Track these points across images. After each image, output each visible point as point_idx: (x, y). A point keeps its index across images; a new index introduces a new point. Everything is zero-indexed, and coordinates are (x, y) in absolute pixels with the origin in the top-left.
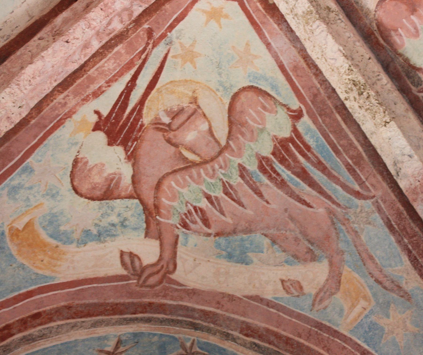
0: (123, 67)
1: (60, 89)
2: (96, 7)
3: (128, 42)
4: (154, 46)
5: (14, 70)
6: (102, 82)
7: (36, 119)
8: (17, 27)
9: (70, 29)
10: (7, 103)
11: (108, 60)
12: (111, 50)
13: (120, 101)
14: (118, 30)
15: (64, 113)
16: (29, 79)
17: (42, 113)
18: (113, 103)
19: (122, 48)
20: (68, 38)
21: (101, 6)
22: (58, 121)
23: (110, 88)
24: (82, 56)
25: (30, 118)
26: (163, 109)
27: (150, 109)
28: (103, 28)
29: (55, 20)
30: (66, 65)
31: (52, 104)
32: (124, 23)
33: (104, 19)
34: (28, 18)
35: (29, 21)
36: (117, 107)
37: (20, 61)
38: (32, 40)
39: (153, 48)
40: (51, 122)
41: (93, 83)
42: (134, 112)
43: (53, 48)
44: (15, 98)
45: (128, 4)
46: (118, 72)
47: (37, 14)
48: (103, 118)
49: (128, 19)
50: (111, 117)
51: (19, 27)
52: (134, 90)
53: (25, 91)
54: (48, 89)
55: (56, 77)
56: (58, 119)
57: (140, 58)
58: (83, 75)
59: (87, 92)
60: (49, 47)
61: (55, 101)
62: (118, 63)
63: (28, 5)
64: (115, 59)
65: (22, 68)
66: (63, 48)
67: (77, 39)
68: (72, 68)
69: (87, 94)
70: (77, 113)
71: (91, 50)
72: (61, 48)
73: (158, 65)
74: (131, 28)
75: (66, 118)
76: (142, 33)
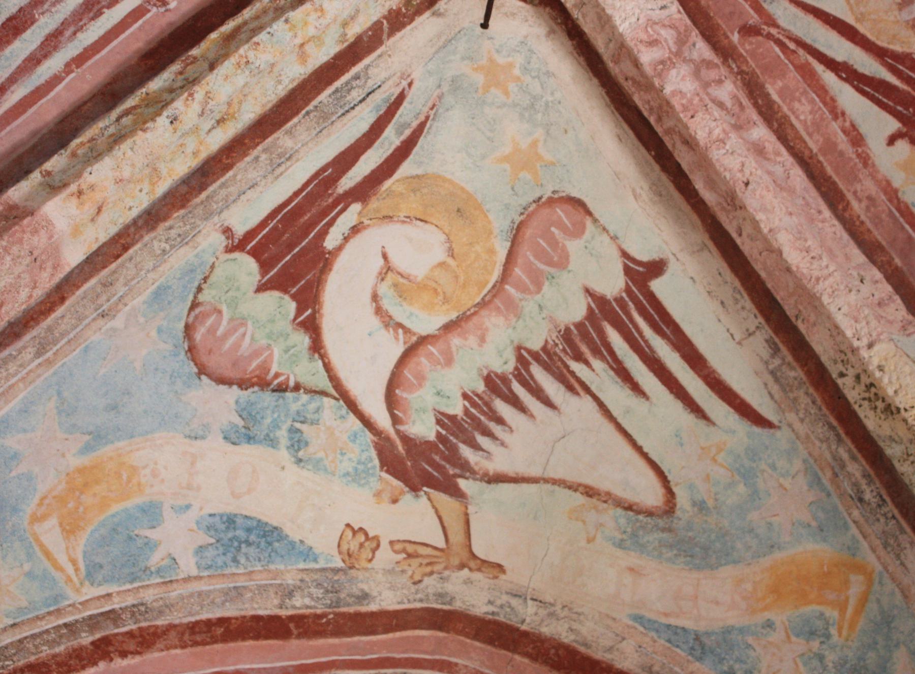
0: (809, 85)
1: (840, 207)
2: (686, 127)
3: (762, 74)
4: (775, 25)
5: (791, 285)
6: (835, 126)
7: (894, 256)
8: (720, 274)
9: (725, 177)
10: (849, 304)
11: (794, 113)
12: (776, 106)
13: (873, 95)
14: (735, 90)
15: (888, 203)
16: (808, 258)
17: (884, 243)
18: (876, 108)
19: (773, 84)
20: (740, 182)
21: (685, 116)
22: (902, 215)
23: (848, 112)
24: (779, 159)
25: (890, 266)
26: (896, 13)
27: (894, 36)
28: (728, 118)
29: (709, 204)
30: (791, 191)
31: (869, 224)
32: (723, 78)
33: (709, 114)
34: (706, 254)
35: (710, 251)
36: (885, 100)
37: (777, 273)
38: (741, 247)
39: (778, 27)
40: (903, 228)
41: (835, 145)
42: (899, 69)
43: (755, 210)
44: (842, 287)
45: (686, 68)
46: (818, 96)
47: (700, 236)
48: (905, 130)
49: (717, 71)
50: (904, 114)
51: (721, 270)
52: (855, 67)
53: (832, 268)
54: (833, 228)
55: (813, 211)
56: (897, 214)
57: (794, 52)
58: (819, 162)
59: (851, 155)
60: (754, 219)
61: (863, 218)
62: (802, 94)
63: (682, 250)
64: (793, 99)
65: (788, 270)
66: (758, 193)
67: (743, 165)
68: (798, 179)
69: (854, 156)
70: (889, 178)
71: (769, 142)
72: (758, 196)
73: (810, 18)
74: (737, 66)
75: (898, 199)
76: (747, 47)
